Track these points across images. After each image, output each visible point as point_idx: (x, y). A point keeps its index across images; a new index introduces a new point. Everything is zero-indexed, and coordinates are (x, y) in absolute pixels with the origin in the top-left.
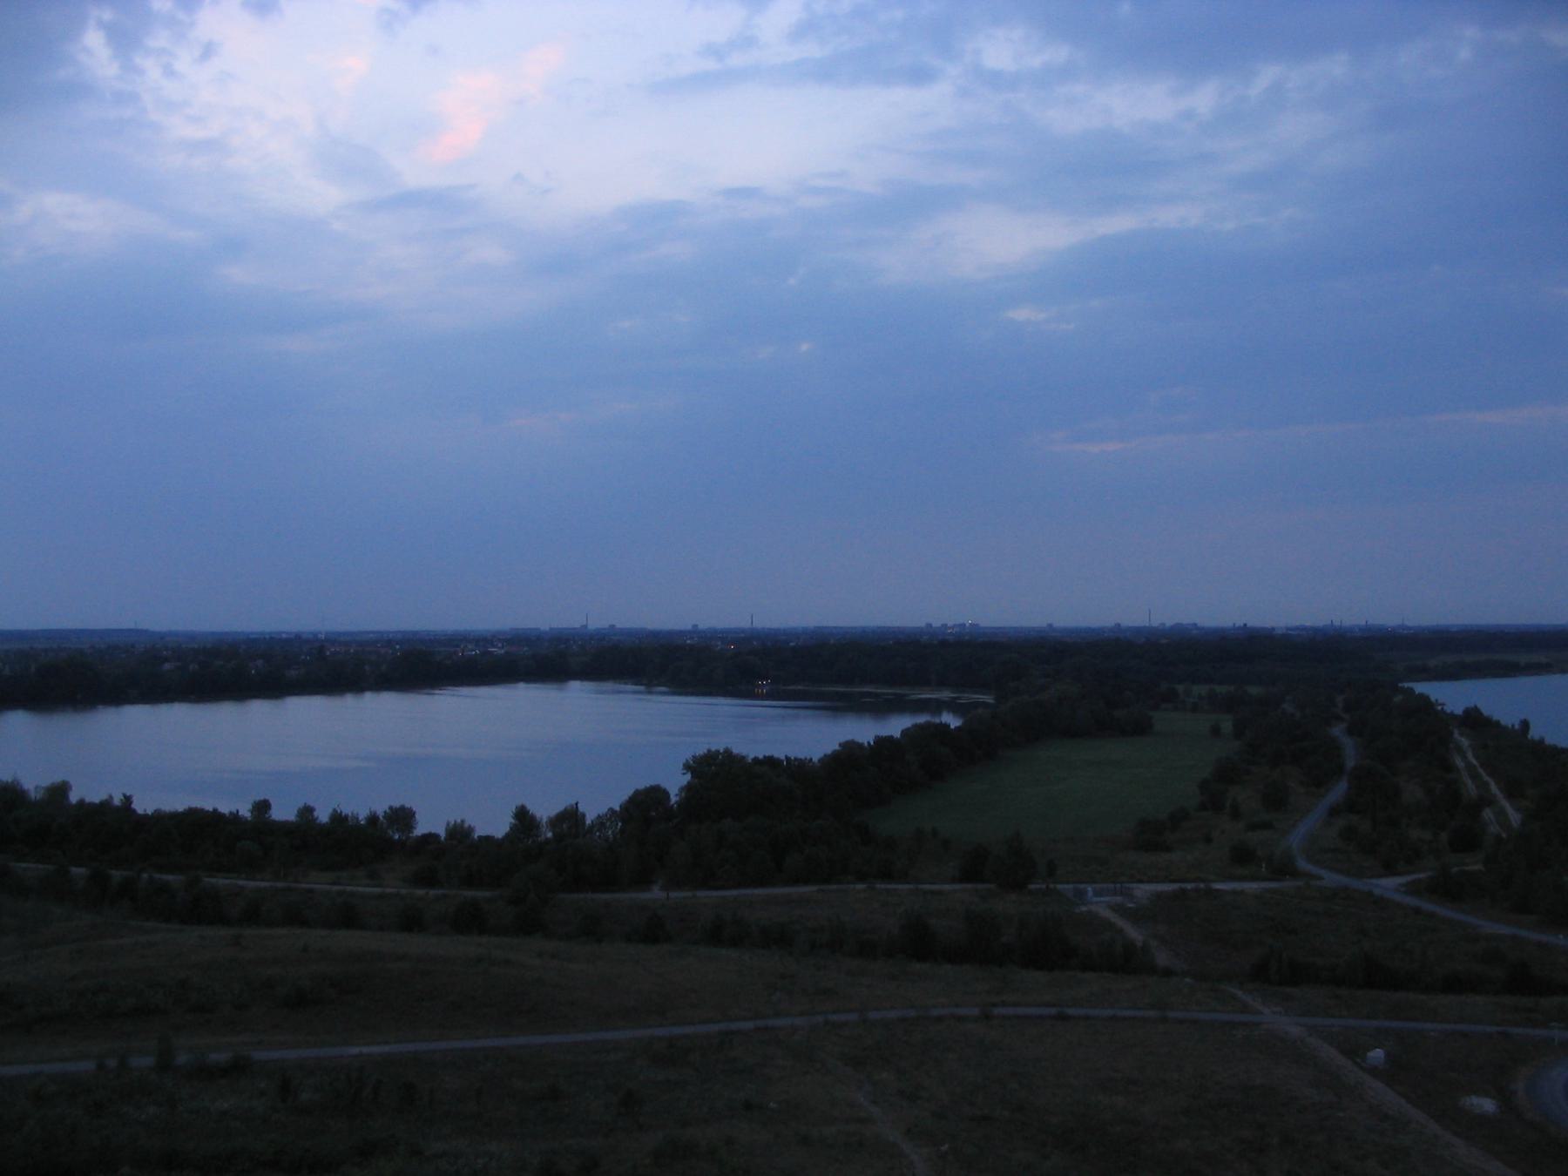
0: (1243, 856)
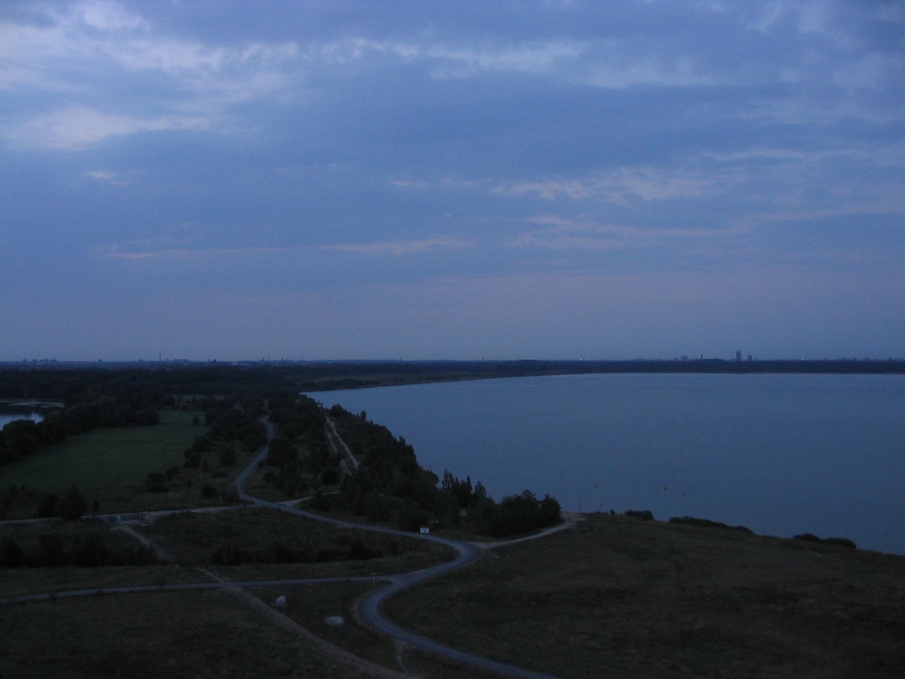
0: (209, 493)
